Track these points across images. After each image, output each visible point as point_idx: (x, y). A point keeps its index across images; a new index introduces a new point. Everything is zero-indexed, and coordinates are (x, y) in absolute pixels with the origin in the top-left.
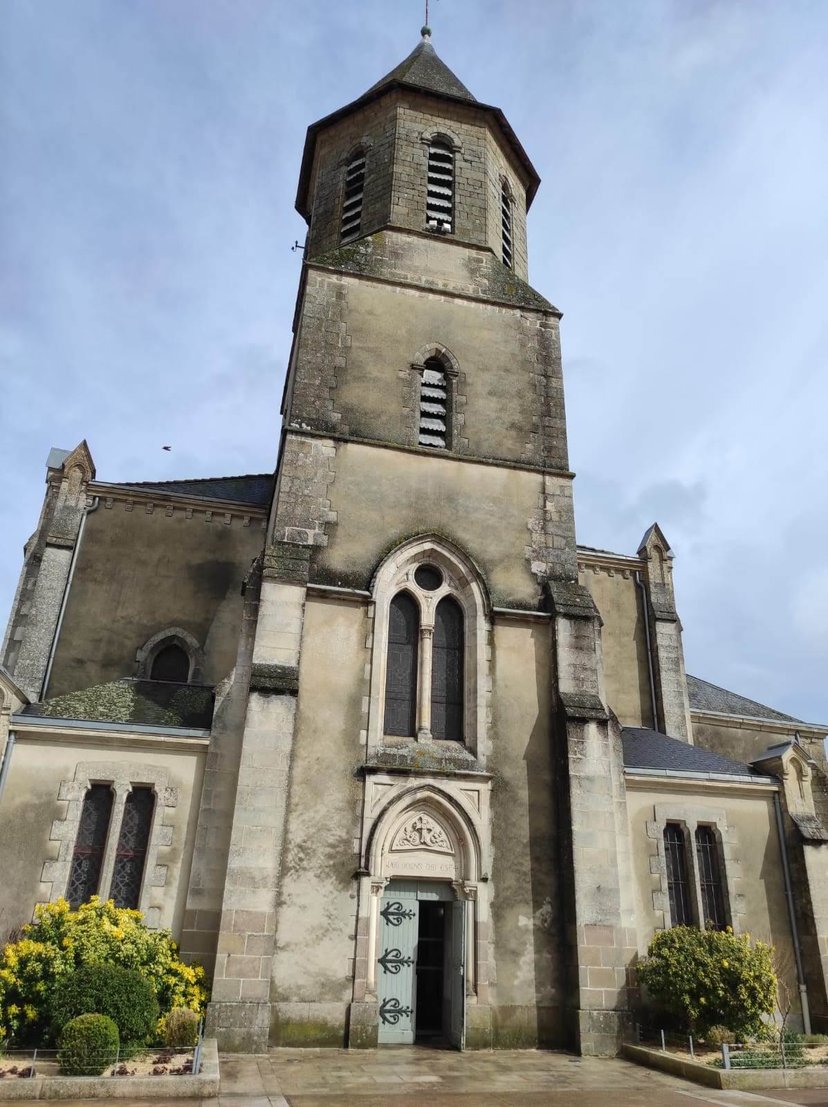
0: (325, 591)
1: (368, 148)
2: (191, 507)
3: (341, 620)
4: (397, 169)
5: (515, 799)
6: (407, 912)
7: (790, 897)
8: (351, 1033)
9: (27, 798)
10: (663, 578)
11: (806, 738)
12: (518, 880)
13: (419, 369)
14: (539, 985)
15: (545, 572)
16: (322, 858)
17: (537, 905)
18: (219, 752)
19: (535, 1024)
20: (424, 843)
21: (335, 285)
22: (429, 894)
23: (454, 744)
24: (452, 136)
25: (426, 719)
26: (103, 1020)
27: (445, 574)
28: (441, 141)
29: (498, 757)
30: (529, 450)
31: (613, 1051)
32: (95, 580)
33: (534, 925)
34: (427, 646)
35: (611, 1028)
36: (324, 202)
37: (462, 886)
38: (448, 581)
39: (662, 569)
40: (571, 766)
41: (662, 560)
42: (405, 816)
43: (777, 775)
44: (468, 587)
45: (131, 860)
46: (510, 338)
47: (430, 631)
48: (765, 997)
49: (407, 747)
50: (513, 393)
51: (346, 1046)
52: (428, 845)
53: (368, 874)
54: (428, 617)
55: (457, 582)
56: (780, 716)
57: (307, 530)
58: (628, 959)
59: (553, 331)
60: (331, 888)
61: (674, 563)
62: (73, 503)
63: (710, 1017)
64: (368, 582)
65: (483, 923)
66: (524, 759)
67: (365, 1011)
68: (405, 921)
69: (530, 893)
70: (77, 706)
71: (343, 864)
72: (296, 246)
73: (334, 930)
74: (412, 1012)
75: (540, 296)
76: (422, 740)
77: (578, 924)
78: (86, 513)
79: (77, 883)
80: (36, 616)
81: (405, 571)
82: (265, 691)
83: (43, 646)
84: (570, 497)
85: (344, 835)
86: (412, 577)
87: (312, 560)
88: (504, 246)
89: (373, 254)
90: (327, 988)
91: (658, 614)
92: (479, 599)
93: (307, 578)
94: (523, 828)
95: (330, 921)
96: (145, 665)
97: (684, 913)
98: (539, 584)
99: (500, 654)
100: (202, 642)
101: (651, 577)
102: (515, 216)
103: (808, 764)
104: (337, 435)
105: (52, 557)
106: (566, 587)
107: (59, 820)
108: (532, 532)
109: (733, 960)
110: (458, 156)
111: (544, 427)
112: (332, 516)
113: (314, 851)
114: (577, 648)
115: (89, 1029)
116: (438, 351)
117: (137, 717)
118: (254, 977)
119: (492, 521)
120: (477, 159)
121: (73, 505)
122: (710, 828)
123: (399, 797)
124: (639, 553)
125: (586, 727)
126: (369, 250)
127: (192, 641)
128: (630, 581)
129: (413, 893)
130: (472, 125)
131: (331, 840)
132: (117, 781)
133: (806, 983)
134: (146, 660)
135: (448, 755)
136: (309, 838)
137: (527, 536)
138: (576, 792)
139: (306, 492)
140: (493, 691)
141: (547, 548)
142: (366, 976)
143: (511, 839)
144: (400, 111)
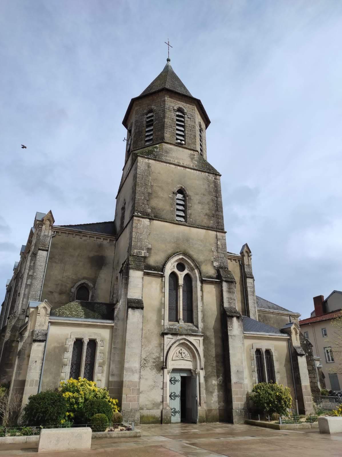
0: (149, 273)
1: (155, 110)
2: (89, 235)
3: (154, 282)
4: (166, 120)
5: (210, 343)
6: (177, 380)
7: (293, 373)
8: (163, 419)
9: (56, 344)
10: (249, 263)
11: (293, 317)
12: (212, 369)
13: (176, 194)
14: (219, 402)
15: (218, 266)
16: (152, 363)
17: (218, 377)
18: (117, 328)
19: (218, 415)
20: (183, 357)
21: (147, 163)
22: (184, 374)
23: (190, 324)
24: (184, 108)
25: (181, 316)
26: (104, 415)
27: (186, 266)
28: (180, 110)
29: (205, 328)
30: (211, 223)
31: (242, 422)
32: (56, 262)
33: (217, 383)
34: (181, 291)
35: (242, 415)
36: (138, 128)
37: (195, 371)
38: (187, 268)
39: (248, 260)
40: (229, 332)
41: (249, 256)
42: (176, 349)
43: (289, 333)
44: (194, 271)
45: (89, 365)
46: (205, 183)
47: (182, 286)
48: (289, 403)
49: (176, 326)
50: (206, 203)
51: (162, 423)
52: (184, 358)
53: (166, 368)
54: (181, 282)
55: (190, 269)
56: (285, 310)
57: (142, 251)
58: (246, 393)
59: (218, 181)
60: (154, 373)
61: (252, 257)
62: (47, 234)
63: (271, 411)
64: (162, 269)
65: (202, 383)
66: (213, 329)
67: (167, 412)
68: (177, 383)
69: (216, 373)
70: (66, 312)
71: (158, 365)
72: (125, 140)
73: (156, 386)
74: (180, 412)
75: (214, 168)
76: (180, 323)
77: (232, 383)
78: (51, 237)
79: (72, 373)
80: (36, 276)
81: (173, 265)
82: (133, 308)
83: (39, 287)
84: (225, 240)
85: (158, 355)
86: (175, 267)
87: (144, 262)
88: (201, 148)
89: (159, 151)
90: (155, 405)
91: (248, 276)
92: (198, 275)
93: (144, 268)
94: (213, 352)
95: (155, 384)
96: (75, 294)
97: (261, 378)
98: (216, 270)
99: (204, 294)
100: (94, 285)
101: (245, 262)
102: (203, 136)
103: (299, 329)
104: (150, 217)
105: (41, 254)
106: (225, 271)
107: (67, 352)
108: (213, 252)
109: (279, 393)
110: (186, 116)
111: (216, 215)
112: (150, 246)
113: (149, 361)
114: (229, 292)
115: (101, 418)
116: (181, 187)
117: (87, 316)
118: (134, 402)
119: (201, 248)
120: (192, 118)
121: (47, 234)
122: (269, 350)
123: (175, 342)
124: (241, 253)
125: (233, 319)
126: (158, 150)
127: (91, 285)
128: (238, 264)
129: (178, 374)
130: (190, 104)
131: (154, 357)
132: (84, 339)
133: (298, 399)
134: (75, 291)
135: (189, 328)
136: (147, 356)
137: (211, 253)
138: (230, 340)
139: (141, 237)
140: (203, 306)
141: (218, 257)
142: (166, 401)
143: (210, 356)
144: (166, 98)
